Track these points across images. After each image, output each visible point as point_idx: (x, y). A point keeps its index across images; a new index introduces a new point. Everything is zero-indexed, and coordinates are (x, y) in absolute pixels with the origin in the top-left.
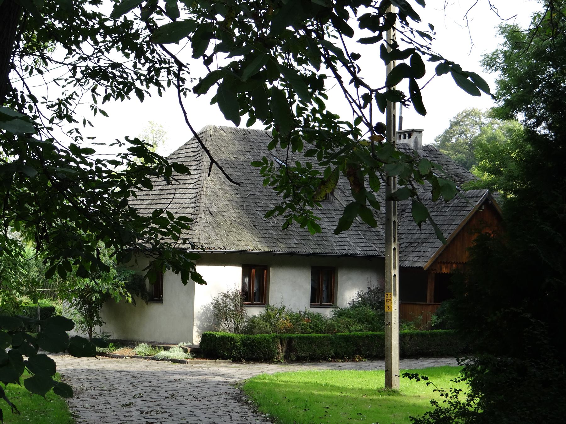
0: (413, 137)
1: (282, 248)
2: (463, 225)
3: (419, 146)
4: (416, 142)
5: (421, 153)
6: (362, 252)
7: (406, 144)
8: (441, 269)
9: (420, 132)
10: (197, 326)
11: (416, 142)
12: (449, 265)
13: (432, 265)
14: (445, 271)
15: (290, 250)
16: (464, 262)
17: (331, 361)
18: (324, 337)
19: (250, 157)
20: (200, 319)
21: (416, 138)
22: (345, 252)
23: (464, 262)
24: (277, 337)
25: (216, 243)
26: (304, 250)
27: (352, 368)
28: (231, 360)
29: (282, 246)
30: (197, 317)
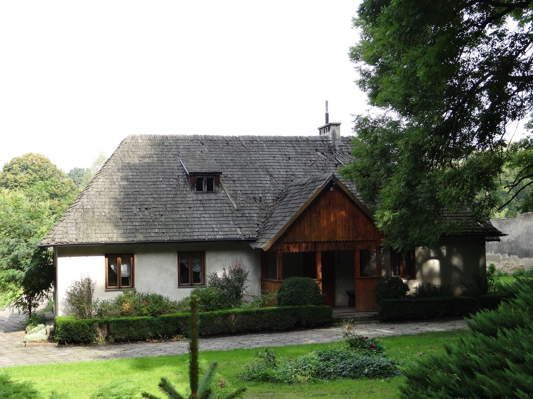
0: (331, 130)
1: (140, 238)
2: (306, 206)
3: (337, 138)
4: (334, 134)
5: (338, 143)
6: (222, 237)
7: (326, 137)
8: (288, 248)
9: (338, 125)
10: (61, 310)
11: (334, 134)
12: (297, 245)
13: (273, 247)
14: (294, 250)
15: (145, 239)
16: (314, 241)
17: (148, 342)
18: (142, 319)
19: (155, 159)
20: (64, 304)
21: (334, 130)
22: (203, 237)
23: (314, 241)
24: (95, 321)
25: (72, 236)
26: (160, 239)
27: (367, 323)
28: (56, 344)
29: (140, 235)
30: (62, 303)
